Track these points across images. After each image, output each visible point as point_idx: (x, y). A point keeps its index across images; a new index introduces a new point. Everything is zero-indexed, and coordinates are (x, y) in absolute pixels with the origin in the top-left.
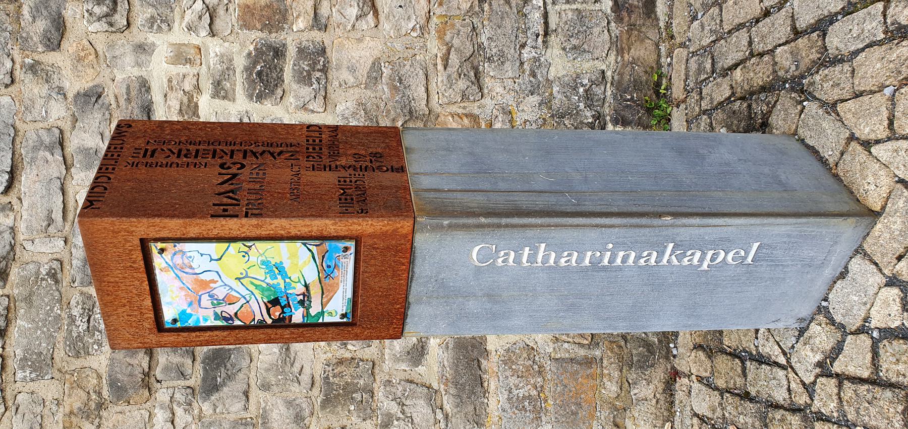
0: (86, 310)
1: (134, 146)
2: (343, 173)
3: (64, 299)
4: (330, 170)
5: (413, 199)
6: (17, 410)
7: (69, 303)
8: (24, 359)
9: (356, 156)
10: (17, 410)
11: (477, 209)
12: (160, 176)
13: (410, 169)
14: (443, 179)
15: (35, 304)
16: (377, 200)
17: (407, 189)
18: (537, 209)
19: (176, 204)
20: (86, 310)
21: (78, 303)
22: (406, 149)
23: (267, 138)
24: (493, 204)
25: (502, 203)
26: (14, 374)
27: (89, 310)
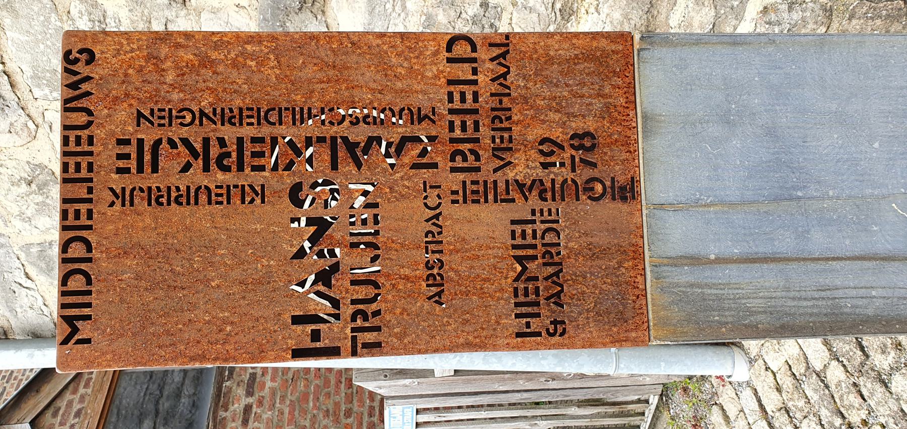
0: (96, 22)
1: (113, 133)
2: (521, 209)
3: (60, 7)
4: (496, 201)
5: (648, 287)
6: (51, 128)
7: (69, 12)
8: (35, 77)
9: (545, 148)
10: (51, 128)
11: (764, 316)
12: (180, 236)
13: (649, 190)
14: (708, 222)
15: (21, 13)
16: (583, 293)
17: (637, 254)
18: (870, 312)
19: (225, 321)
20: (96, 22)
21: (80, 12)
22: (645, 117)
23: (373, 90)
24: (794, 299)
25: (809, 294)
26: (30, 91)
27: (100, 22)
